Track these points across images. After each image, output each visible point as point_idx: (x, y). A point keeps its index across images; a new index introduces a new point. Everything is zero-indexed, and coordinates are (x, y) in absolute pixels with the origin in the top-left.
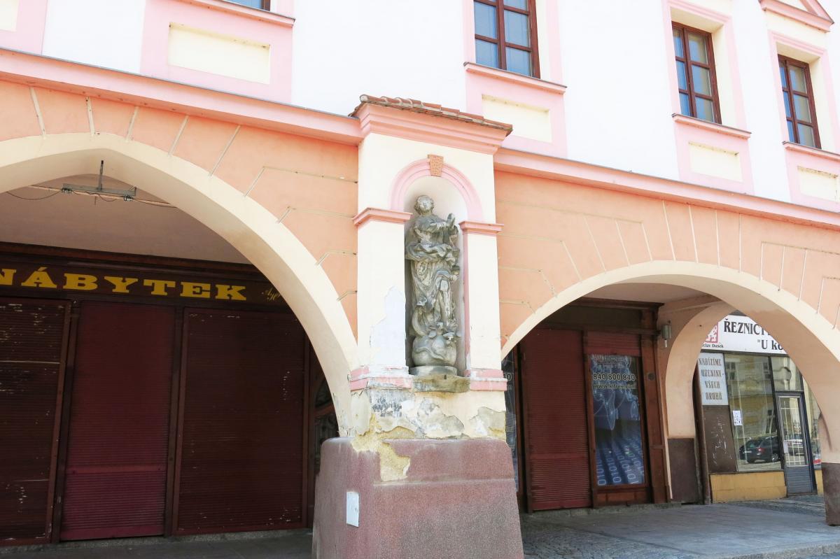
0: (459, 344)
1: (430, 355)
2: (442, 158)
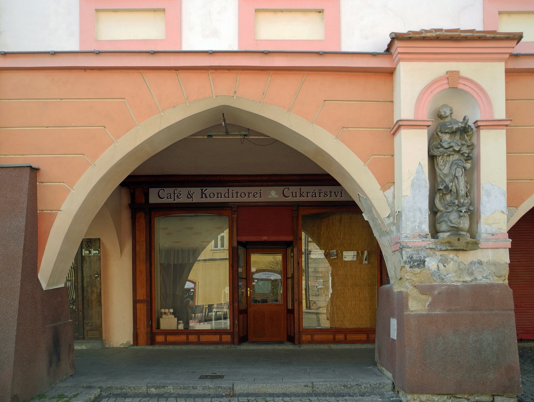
0: (473, 214)
1: (447, 225)
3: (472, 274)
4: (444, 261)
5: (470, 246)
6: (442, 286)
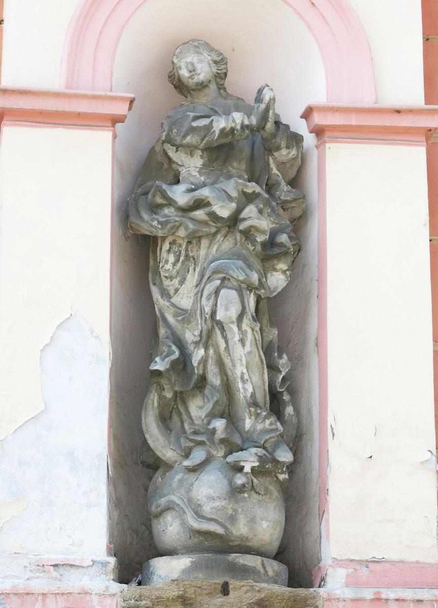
1: (184, 523)
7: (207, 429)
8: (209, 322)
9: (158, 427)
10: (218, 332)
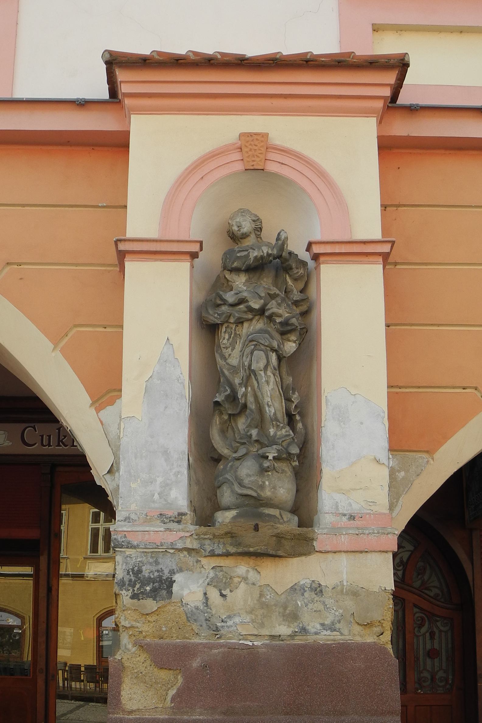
0: (303, 463)
1: (233, 491)
2: (267, 135)
3: (293, 616)
4: (223, 584)
5: (287, 545)
6: (211, 647)
7: (247, 435)
8: (247, 371)
9: (219, 435)
10: (253, 376)
